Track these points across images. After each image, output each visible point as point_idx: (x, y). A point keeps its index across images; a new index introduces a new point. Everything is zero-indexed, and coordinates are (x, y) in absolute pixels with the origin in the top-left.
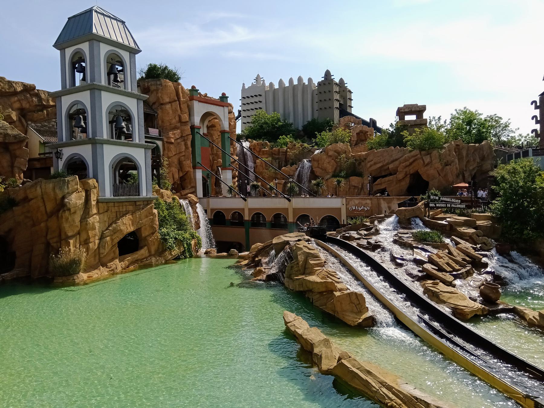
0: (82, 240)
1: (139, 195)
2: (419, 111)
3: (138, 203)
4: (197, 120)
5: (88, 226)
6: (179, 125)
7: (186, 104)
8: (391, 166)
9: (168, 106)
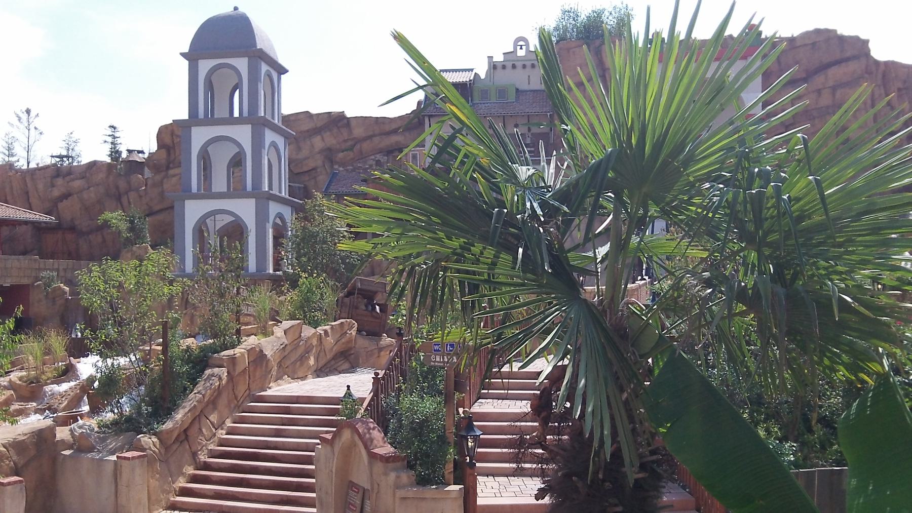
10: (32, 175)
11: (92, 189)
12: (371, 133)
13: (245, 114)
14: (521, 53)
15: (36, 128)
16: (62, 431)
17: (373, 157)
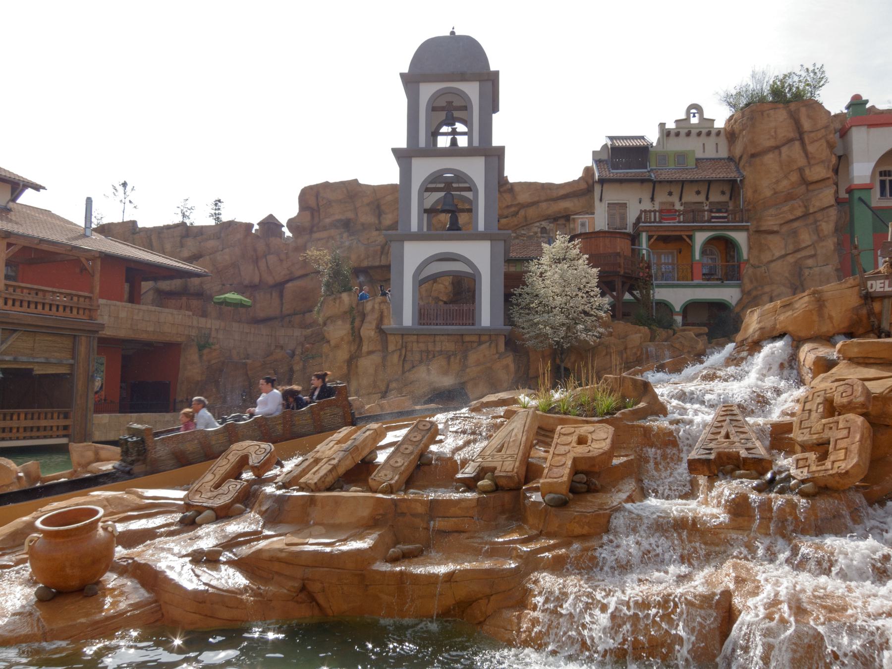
1: (473, 324)
3: (467, 339)
6: (803, 188)
7: (823, 141)
9: (769, 158)
10: (159, 233)
11: (227, 250)
12: (536, 199)
13: (476, 143)
14: (694, 121)
15: (130, 202)
16: (171, 568)
17: (538, 224)
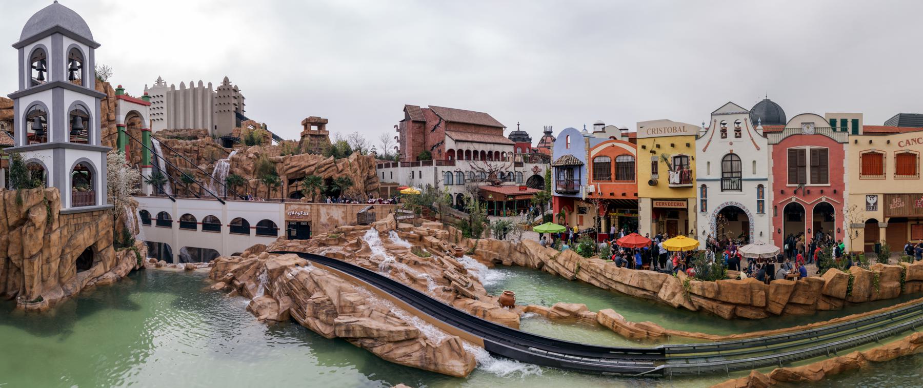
0: (44, 258)
1: (94, 204)
2: (321, 123)
4: (122, 119)
5: (52, 243)
6: (107, 123)
8: (307, 171)
